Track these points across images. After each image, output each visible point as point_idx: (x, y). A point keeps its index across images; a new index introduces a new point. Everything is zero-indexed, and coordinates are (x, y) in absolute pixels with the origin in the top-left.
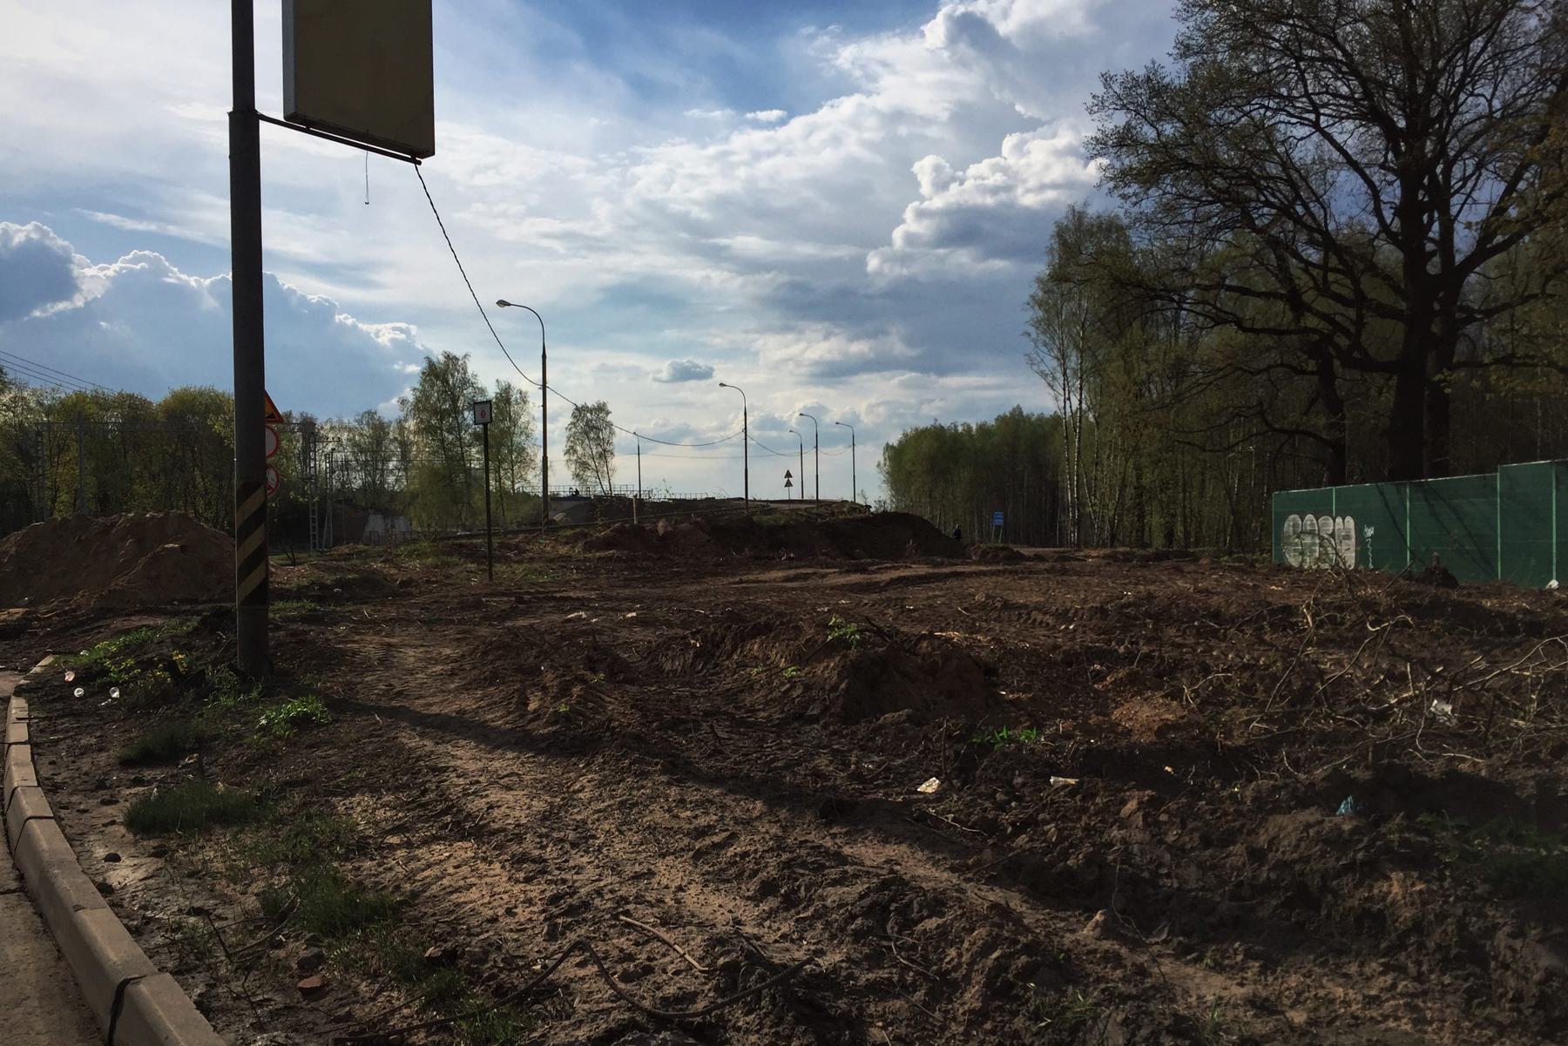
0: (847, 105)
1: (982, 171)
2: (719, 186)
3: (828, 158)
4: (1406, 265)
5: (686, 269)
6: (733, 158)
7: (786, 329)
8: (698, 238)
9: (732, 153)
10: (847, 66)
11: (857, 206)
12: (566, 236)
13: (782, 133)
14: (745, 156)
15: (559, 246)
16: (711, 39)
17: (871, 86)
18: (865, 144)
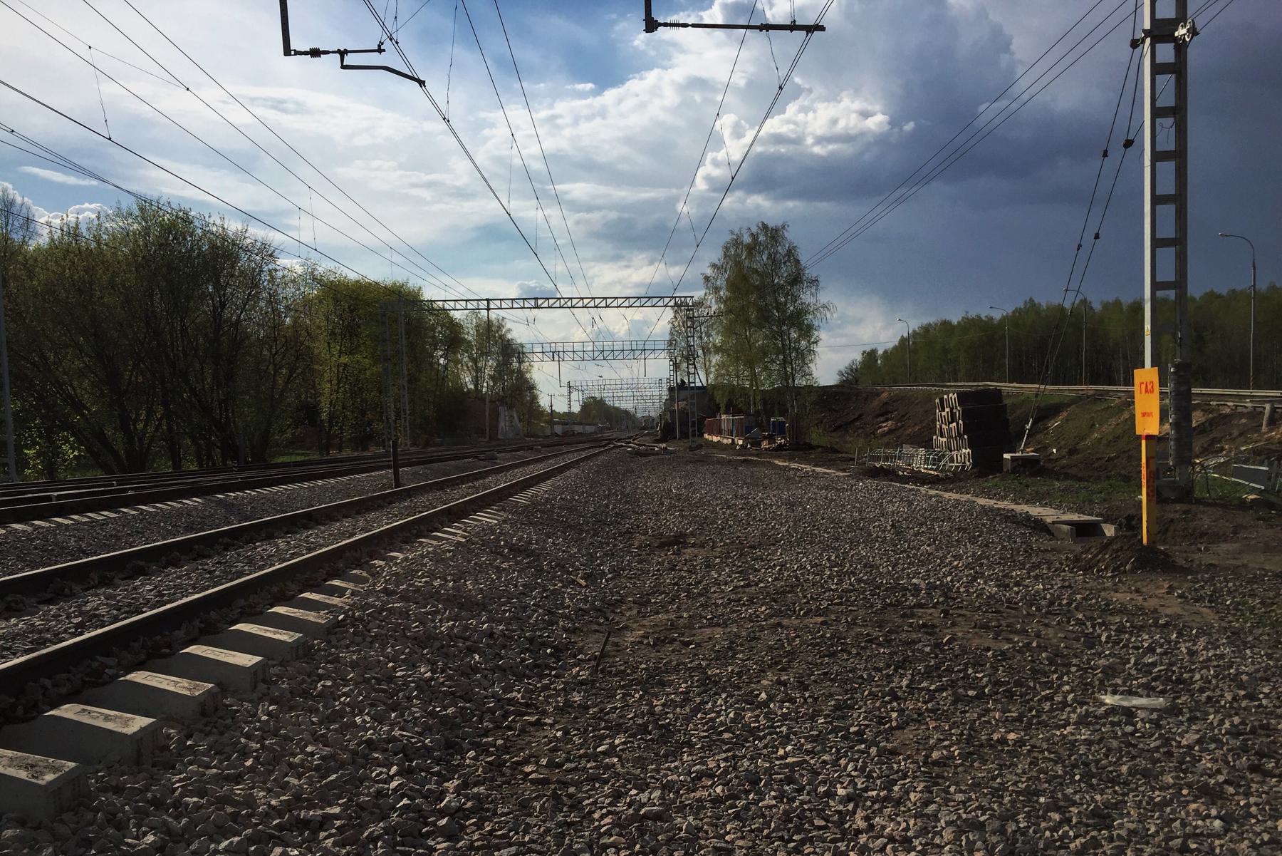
0: (652, 76)
1: (774, 125)
2: (550, 144)
3: (638, 121)
4: (810, 388)
5: (531, 209)
6: (559, 121)
7: (616, 258)
8: (538, 183)
9: (560, 116)
10: (642, 47)
11: (663, 155)
12: (429, 185)
13: (598, 101)
14: (568, 120)
15: (426, 194)
16: (560, 27)
17: (665, 63)
18: (664, 109)
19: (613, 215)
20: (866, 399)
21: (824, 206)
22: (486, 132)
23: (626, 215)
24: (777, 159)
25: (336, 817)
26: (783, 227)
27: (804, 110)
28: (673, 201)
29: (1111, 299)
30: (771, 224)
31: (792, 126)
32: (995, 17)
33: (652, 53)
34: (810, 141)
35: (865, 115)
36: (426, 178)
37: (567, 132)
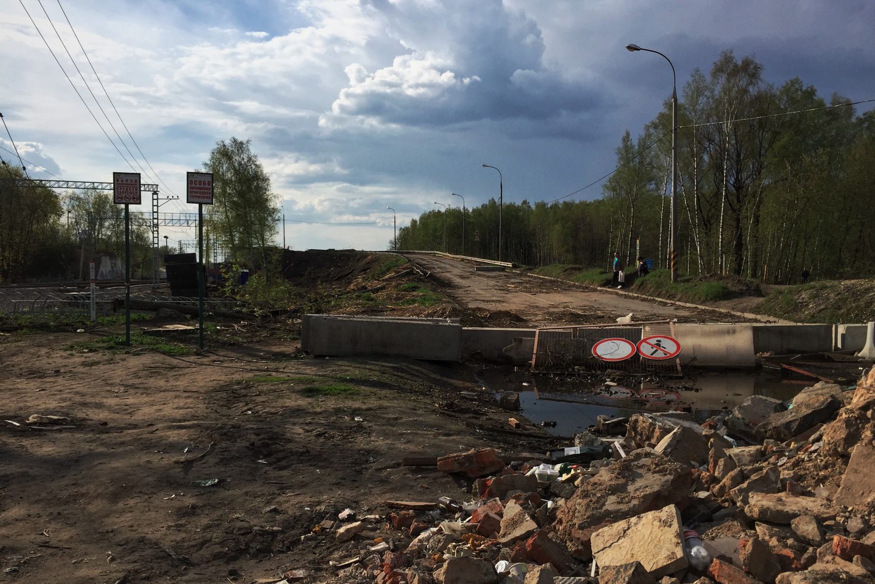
0: (306, 32)
1: (384, 74)
2: (231, 72)
3: (295, 62)
6: (239, 57)
7: (273, 156)
9: (238, 54)
10: (303, 11)
13: (268, 45)
15: (133, 101)
19: (272, 126)
20: (359, 260)
21: (416, 129)
22: (183, 60)
23: (280, 127)
24: (384, 96)
25: (334, 559)
26: (248, 142)
27: (405, 64)
28: (316, 120)
29: (540, 201)
30: (240, 139)
31: (394, 76)
32: (530, 16)
33: (310, 15)
34: (405, 86)
35: (442, 71)
36: (132, 89)
37: (244, 65)
